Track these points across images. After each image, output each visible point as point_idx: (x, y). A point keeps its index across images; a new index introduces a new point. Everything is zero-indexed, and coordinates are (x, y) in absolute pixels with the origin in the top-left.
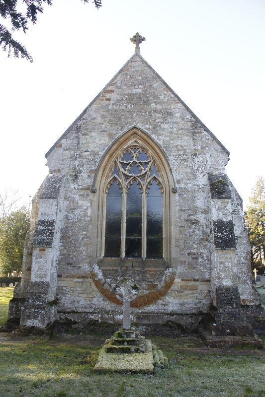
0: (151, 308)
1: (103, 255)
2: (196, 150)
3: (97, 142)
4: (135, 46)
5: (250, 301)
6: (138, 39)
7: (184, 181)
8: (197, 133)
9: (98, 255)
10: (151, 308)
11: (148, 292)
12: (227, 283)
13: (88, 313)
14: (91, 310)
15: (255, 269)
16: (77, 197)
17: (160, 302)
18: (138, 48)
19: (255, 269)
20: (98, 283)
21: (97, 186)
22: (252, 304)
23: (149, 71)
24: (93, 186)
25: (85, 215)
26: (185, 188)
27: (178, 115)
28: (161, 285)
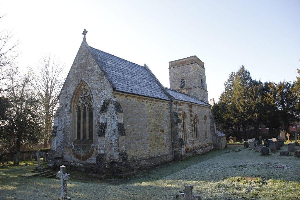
0: (87, 161)
1: (76, 138)
2: (102, 88)
3: (72, 89)
4: (83, 36)
5: (119, 160)
6: (85, 33)
7: (97, 104)
8: (102, 79)
9: (74, 139)
10: (87, 161)
11: (86, 154)
12: (102, 152)
13: (70, 162)
14: (71, 161)
15: (288, 134)
16: (67, 115)
17: (90, 158)
18: (85, 36)
19: (288, 134)
20: (73, 150)
21: (72, 110)
22: (119, 162)
23: (71, 73)
24: (70, 109)
25: (69, 122)
26: (97, 107)
27: (96, 71)
28: (90, 152)
